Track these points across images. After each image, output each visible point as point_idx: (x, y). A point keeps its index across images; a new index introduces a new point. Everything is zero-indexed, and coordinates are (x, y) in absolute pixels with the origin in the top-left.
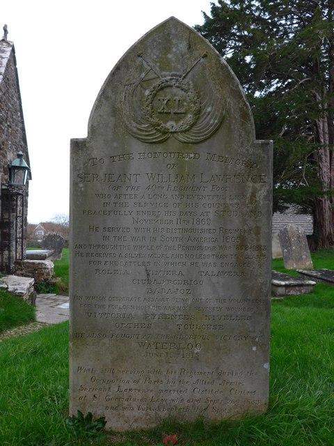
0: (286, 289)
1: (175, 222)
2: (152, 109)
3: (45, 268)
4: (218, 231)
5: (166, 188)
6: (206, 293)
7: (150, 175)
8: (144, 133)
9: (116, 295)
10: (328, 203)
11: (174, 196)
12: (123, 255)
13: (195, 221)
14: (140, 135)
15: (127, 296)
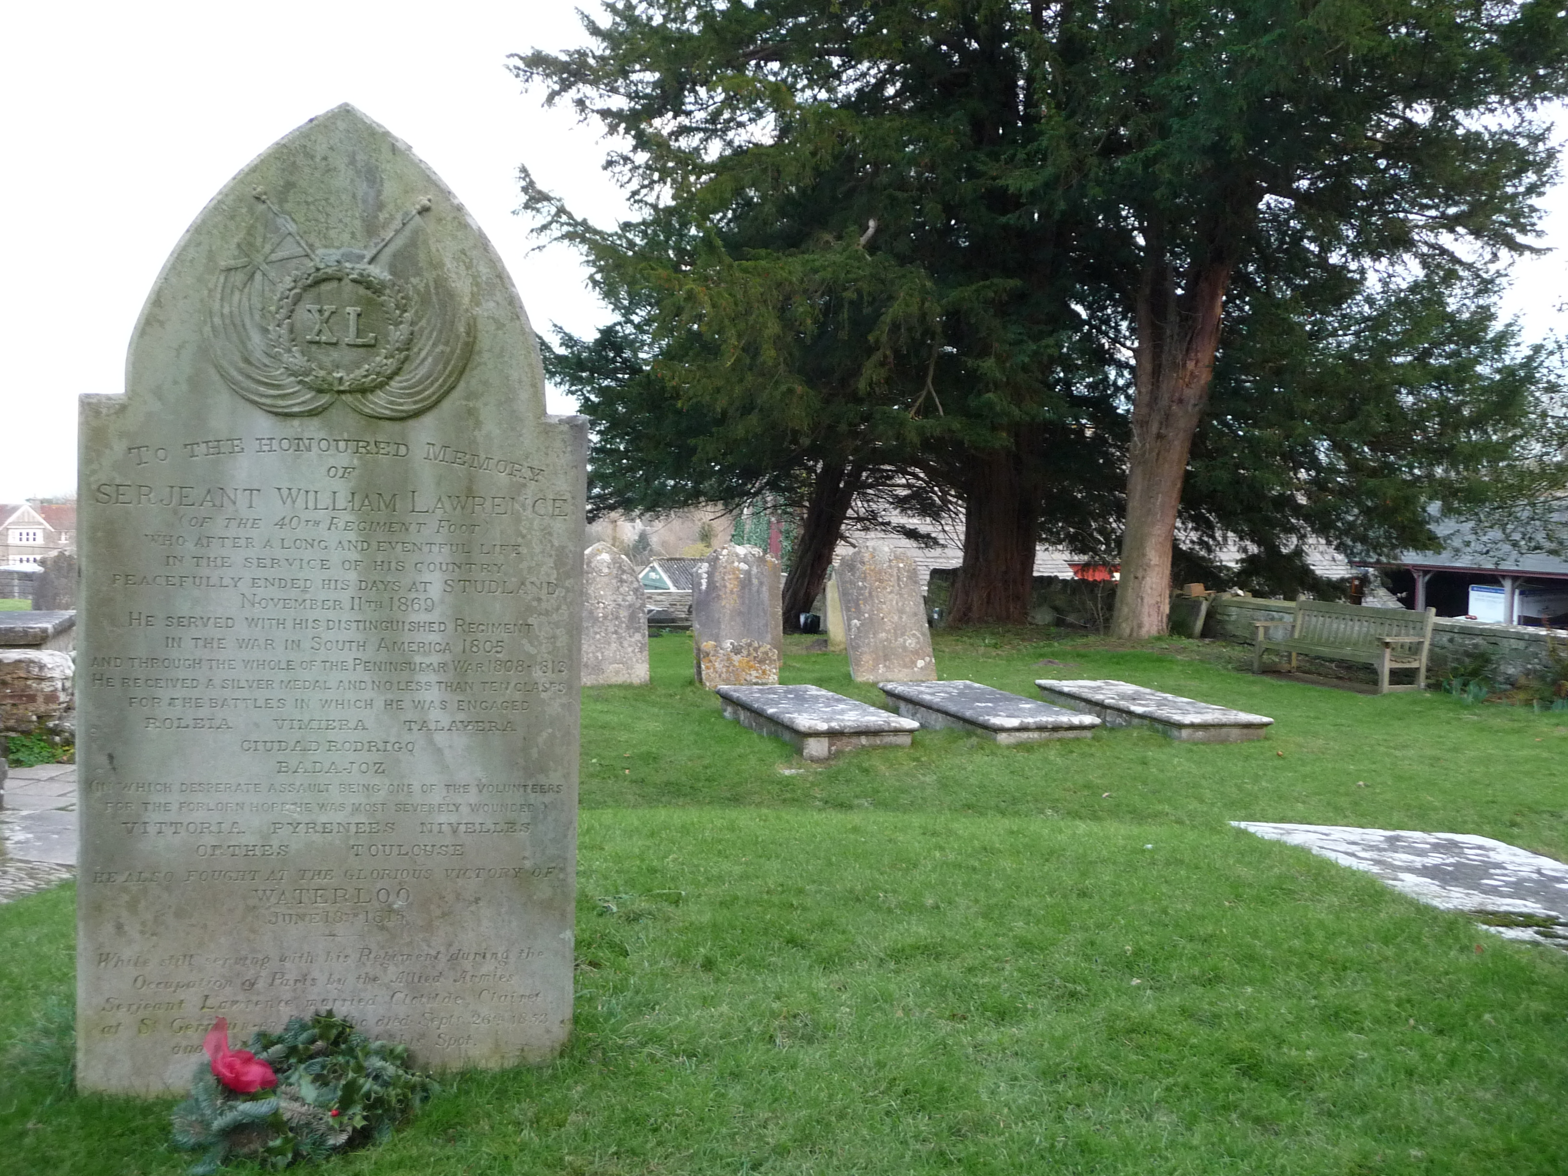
0: (318, 300)
1: (347, 605)
2: (291, 331)
3: (41, 679)
4: (451, 626)
5: (324, 526)
6: (421, 773)
7: (285, 492)
8: (436, 385)
9: (196, 780)
10: (1276, 870)
11: (346, 545)
12: (217, 682)
13: (396, 603)
14: (263, 396)
15: (220, 787)
